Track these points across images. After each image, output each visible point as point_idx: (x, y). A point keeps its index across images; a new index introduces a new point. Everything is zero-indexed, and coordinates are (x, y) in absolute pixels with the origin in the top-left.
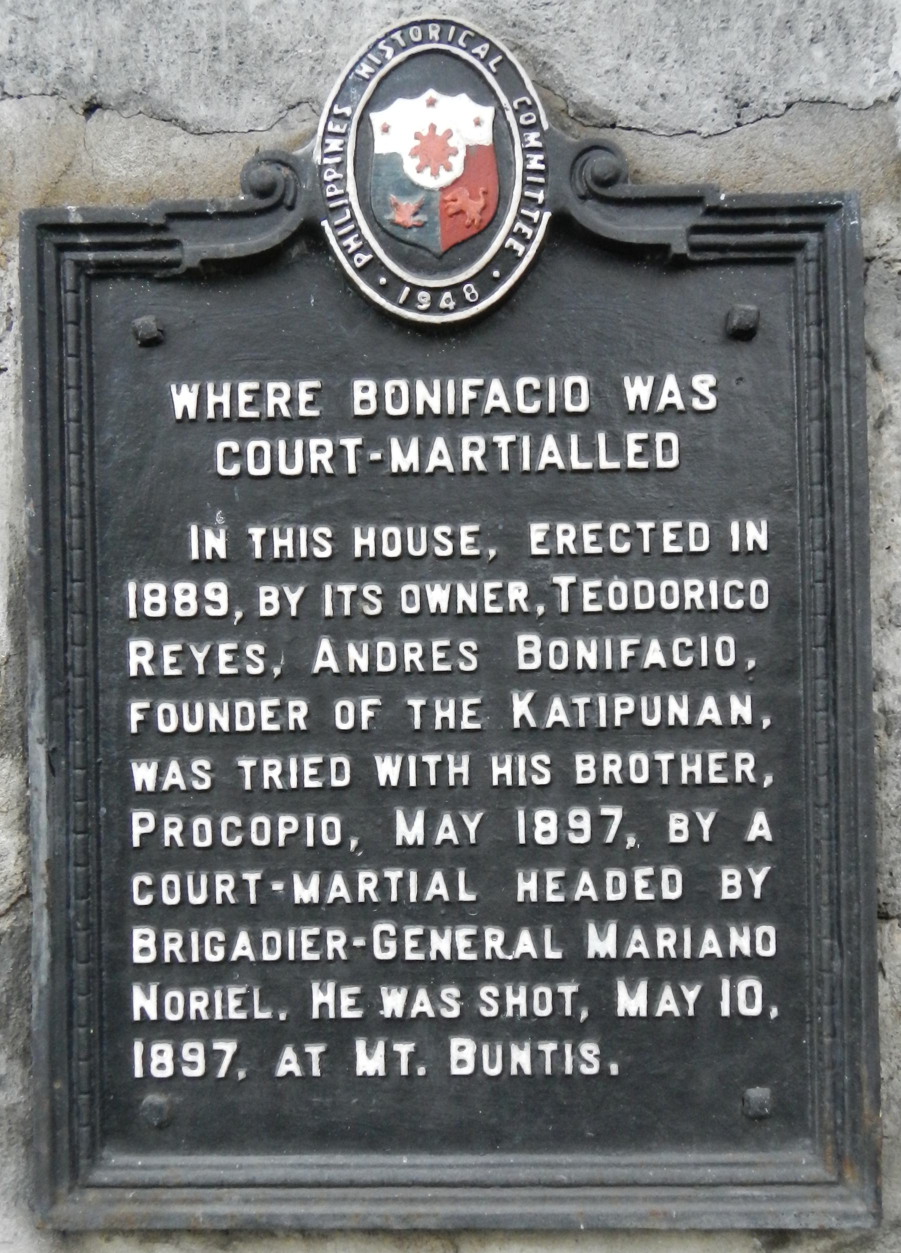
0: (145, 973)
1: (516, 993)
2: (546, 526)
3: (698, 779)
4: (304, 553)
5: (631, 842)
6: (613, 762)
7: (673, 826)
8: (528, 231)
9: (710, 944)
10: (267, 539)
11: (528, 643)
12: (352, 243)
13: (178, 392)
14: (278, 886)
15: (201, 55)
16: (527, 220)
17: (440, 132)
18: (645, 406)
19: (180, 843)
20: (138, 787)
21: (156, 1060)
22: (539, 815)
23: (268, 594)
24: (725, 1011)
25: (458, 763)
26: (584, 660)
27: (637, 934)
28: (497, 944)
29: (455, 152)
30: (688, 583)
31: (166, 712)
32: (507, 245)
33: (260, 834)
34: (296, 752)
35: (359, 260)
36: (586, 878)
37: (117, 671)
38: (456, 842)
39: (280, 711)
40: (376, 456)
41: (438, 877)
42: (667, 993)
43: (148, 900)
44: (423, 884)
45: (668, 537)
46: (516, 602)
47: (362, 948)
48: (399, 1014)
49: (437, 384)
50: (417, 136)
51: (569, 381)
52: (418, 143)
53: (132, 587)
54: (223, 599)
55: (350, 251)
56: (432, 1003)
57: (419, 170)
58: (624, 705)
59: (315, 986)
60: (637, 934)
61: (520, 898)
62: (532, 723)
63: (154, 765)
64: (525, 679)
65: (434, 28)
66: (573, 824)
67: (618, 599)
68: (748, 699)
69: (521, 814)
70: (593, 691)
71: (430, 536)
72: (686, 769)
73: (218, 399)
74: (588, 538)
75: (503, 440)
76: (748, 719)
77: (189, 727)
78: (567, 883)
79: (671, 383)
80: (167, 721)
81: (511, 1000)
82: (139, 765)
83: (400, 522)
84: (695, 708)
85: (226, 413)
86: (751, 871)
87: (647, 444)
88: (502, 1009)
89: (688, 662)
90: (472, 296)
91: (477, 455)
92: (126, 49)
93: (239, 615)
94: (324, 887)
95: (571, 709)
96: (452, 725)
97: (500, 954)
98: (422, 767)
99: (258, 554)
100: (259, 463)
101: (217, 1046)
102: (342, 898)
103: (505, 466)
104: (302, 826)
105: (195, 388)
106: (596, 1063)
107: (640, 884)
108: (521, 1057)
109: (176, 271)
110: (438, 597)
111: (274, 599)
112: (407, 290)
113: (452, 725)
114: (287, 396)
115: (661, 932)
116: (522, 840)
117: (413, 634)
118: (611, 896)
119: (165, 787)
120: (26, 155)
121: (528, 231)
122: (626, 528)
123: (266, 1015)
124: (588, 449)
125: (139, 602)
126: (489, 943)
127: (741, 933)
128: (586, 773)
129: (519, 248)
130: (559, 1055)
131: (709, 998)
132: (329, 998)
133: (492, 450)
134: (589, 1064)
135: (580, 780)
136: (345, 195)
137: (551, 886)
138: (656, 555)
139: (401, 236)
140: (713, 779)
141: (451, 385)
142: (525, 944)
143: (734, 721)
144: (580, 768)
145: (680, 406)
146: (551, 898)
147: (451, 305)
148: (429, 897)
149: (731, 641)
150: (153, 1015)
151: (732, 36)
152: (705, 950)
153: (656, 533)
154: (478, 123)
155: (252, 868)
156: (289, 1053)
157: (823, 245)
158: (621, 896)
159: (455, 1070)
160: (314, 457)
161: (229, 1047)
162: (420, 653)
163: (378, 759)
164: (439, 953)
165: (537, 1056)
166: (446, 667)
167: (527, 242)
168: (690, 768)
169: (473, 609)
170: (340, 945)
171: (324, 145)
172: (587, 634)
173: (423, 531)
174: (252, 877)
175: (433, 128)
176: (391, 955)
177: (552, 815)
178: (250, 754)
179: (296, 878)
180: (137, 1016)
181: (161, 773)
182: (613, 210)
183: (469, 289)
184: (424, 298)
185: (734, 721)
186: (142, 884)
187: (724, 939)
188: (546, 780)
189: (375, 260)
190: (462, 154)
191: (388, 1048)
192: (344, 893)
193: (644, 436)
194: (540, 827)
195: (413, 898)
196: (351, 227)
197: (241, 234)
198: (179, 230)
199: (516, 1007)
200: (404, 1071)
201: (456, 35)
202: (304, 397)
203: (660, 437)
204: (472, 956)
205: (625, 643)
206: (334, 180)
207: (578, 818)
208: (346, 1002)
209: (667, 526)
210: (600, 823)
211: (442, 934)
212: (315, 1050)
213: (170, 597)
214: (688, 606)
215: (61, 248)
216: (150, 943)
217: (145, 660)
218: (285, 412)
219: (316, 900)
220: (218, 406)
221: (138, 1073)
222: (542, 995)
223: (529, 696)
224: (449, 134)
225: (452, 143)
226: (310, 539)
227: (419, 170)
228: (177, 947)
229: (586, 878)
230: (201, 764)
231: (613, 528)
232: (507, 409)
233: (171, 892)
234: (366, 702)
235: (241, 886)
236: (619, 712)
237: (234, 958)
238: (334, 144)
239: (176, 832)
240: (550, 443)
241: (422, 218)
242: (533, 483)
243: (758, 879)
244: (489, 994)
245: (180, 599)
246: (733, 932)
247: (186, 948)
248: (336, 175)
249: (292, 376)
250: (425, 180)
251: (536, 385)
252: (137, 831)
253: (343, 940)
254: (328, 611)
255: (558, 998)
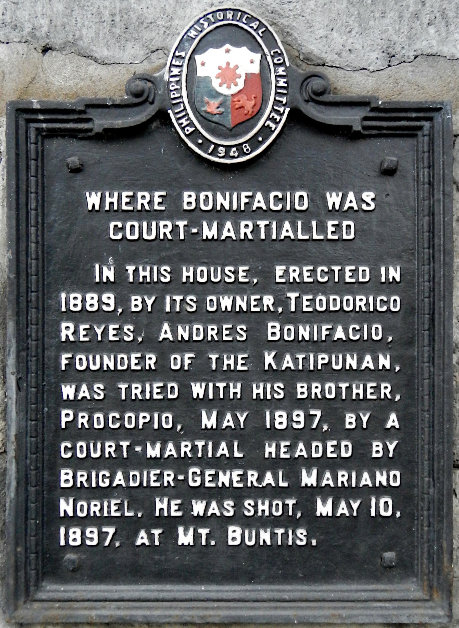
0: (66, 492)
1: (263, 503)
2: (284, 268)
3: (361, 397)
4: (155, 280)
5: (325, 428)
6: (317, 387)
7: (348, 420)
8: (278, 118)
9: (366, 480)
10: (136, 271)
11: (273, 327)
12: (184, 122)
13: (90, 196)
14: (138, 449)
15: (105, 24)
16: (277, 112)
17: (232, 66)
18: (337, 208)
19: (87, 426)
20: (65, 398)
21: (72, 536)
22: (277, 414)
23: (136, 300)
24: (373, 514)
25: (235, 387)
26: (303, 336)
27: (328, 475)
28: (254, 479)
29: (240, 77)
30: (358, 298)
31: (81, 359)
32: (266, 125)
33: (130, 422)
34: (149, 380)
35: (188, 130)
36: (301, 446)
37: (55, 338)
38: (233, 427)
39: (142, 359)
40: (195, 230)
41: (223, 445)
42: (343, 504)
43: (69, 455)
44: (216, 448)
45: (348, 274)
46: (268, 306)
47: (182, 480)
48: (201, 514)
49: (228, 194)
50: (220, 68)
51: (298, 194)
52: (220, 71)
53: (63, 295)
54: (112, 302)
55: (183, 126)
56: (219, 508)
57: (220, 85)
58: (323, 359)
59: (157, 500)
60: (328, 475)
61: (267, 456)
62: (275, 368)
63: (74, 387)
64: (271, 345)
65: (230, 13)
66: (295, 419)
67: (321, 305)
68: (388, 356)
69: (268, 413)
70: (307, 351)
71: (223, 271)
72: (355, 391)
73: (111, 200)
74: (306, 274)
75: (262, 224)
76: (388, 367)
77: (92, 367)
78: (291, 448)
79: (351, 196)
80: (81, 364)
81: (260, 507)
82: (65, 386)
83: (207, 264)
84: (360, 361)
85: (116, 208)
86: (388, 443)
87: (338, 227)
88: (256, 512)
89: (357, 337)
90: (247, 150)
91: (248, 231)
92: (65, 20)
93: (120, 310)
94: (163, 450)
95: (295, 360)
96: (232, 368)
97: (256, 484)
98: (216, 388)
99: (131, 280)
100: (132, 233)
101: (105, 529)
102: (172, 455)
103: (263, 237)
104: (152, 418)
105: (99, 194)
106: (305, 539)
107: (330, 449)
108: (265, 536)
109: (90, 134)
110: (226, 302)
111: (139, 303)
112: (213, 146)
113: (232, 368)
114: (148, 199)
115: (340, 473)
116: (268, 427)
117: (212, 322)
118: (314, 455)
119: (79, 398)
120: (10, 73)
121: (278, 118)
122: (326, 269)
123: (131, 514)
124: (307, 229)
125: (67, 303)
126: (250, 479)
127: (382, 474)
128: (302, 393)
129: (273, 126)
130: (285, 535)
131: (365, 507)
132: (165, 506)
133: (256, 228)
134: (301, 540)
135: (299, 396)
136: (181, 97)
137: (283, 450)
138: (341, 283)
139: (210, 119)
140: (369, 397)
141: (235, 195)
142: (269, 479)
143: (381, 368)
144: (299, 390)
145: (356, 208)
146: (283, 456)
147: (236, 154)
148: (218, 455)
149: (380, 327)
150: (71, 514)
151: (387, 21)
152: (363, 483)
153: (342, 272)
154: (252, 62)
155: (125, 439)
156: (143, 533)
157: (432, 127)
158: (319, 455)
159: (231, 543)
160: (162, 231)
161: (111, 530)
162: (216, 331)
163: (193, 385)
164: (223, 483)
165: (273, 535)
166: (230, 339)
167: (277, 123)
168: (358, 391)
169: (245, 309)
170: (171, 479)
171: (170, 71)
172: (305, 323)
173: (219, 269)
174: (125, 444)
175: (228, 64)
176: (198, 484)
177: (284, 414)
178: (125, 381)
179: (148, 445)
180: (62, 514)
181: (77, 390)
182: (322, 108)
183: (245, 146)
184: (222, 151)
185: (381, 368)
186: (66, 447)
187: (373, 478)
188: (281, 396)
189: (196, 129)
190: (243, 77)
191: (195, 531)
192: (174, 453)
193: (336, 223)
194: (278, 420)
195: (210, 455)
196: (184, 113)
197: (124, 116)
198: (92, 113)
199: (263, 511)
200: (204, 543)
201: (241, 17)
202: (157, 200)
203: (345, 223)
204: (241, 485)
205: (324, 328)
206: (175, 90)
207: (298, 415)
208: (174, 508)
209: (348, 268)
210: (309, 418)
211: (225, 474)
212: (156, 532)
213: (84, 300)
214: (358, 309)
215: (29, 121)
216: (70, 477)
217: (70, 333)
218: (147, 207)
219: (158, 456)
220: (111, 204)
221: (62, 543)
222: (277, 505)
223: (273, 354)
224: (237, 67)
225: (238, 72)
226: (159, 272)
227: (220, 85)
228: (84, 479)
229: (301, 446)
230: (98, 386)
231: (319, 269)
232: (265, 208)
233: (81, 451)
234: (187, 356)
235: (119, 448)
236: (320, 362)
237: (114, 485)
238: (176, 71)
239: (85, 421)
240: (287, 225)
241: (221, 110)
242: (278, 246)
243: (391, 447)
244: (249, 504)
245: (89, 302)
246: (378, 474)
247: (89, 479)
248: (176, 87)
249: (151, 189)
250: (224, 90)
251: (280, 196)
252: (64, 420)
253: (173, 476)
254: (168, 309)
255: (285, 506)
